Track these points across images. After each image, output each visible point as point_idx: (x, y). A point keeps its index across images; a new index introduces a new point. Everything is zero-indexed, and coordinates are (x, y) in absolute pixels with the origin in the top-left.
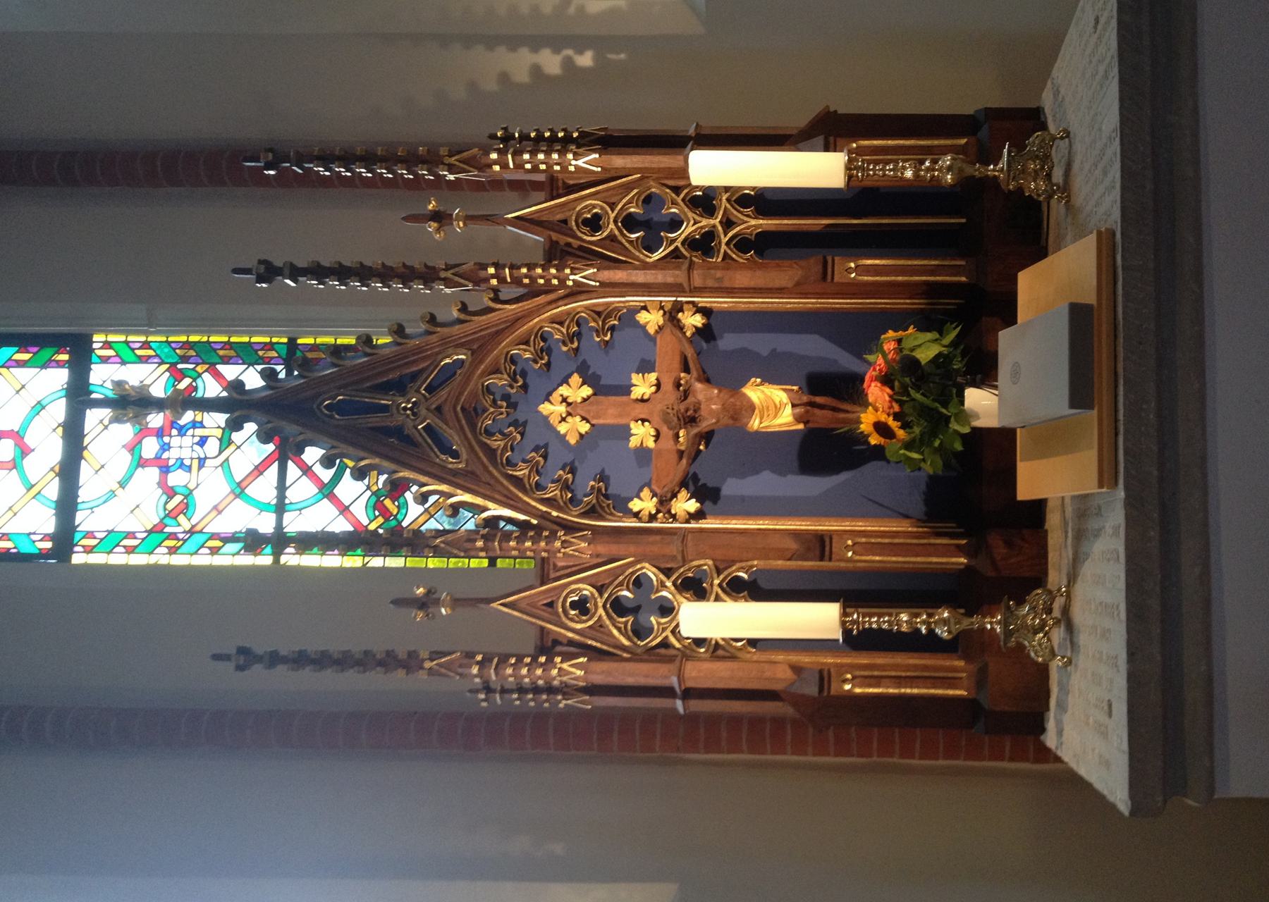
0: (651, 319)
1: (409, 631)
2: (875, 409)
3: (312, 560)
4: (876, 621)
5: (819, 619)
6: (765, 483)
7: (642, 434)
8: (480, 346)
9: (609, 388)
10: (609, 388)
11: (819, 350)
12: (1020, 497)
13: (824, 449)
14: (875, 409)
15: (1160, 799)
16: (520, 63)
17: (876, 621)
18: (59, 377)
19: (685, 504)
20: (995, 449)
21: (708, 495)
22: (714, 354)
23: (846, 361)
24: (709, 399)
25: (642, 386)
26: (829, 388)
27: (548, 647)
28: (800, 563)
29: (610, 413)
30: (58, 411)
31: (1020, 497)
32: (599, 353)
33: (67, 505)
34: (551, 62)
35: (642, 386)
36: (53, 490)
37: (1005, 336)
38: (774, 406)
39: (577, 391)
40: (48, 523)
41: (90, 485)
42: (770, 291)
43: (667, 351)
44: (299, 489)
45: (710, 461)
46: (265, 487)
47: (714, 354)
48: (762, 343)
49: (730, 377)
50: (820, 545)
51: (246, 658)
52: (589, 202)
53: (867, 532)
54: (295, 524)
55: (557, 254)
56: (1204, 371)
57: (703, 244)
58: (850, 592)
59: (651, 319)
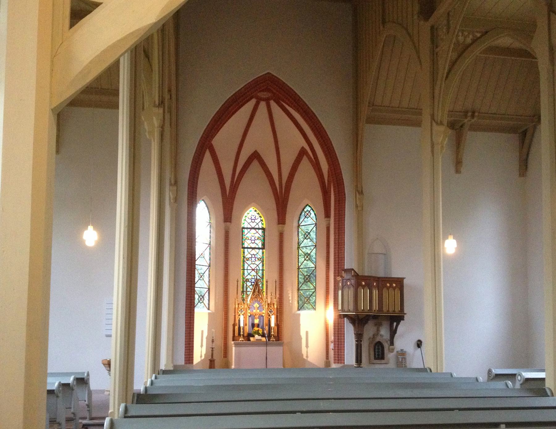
0: (263, 311)
2: (256, 329)
6: (251, 320)
7: (254, 311)
8: (261, 298)
12: (90, 228)
13: (253, 325)
14: (256, 329)
15: (441, 138)
16: (290, 295)
18: (260, 246)
19: (249, 315)
20: (253, 336)
22: (261, 316)
23: (260, 326)
24: (257, 316)
25: (258, 311)
26: (258, 326)
27: (238, 304)
29: (256, 308)
30: (257, 247)
31: (90, 228)
33: (247, 248)
34: (290, 298)
35: (258, 311)
36: (249, 246)
37: (455, 375)
38: (256, 321)
39: (258, 306)
40: (246, 246)
41: (250, 250)
42: (266, 321)
43: (261, 313)
45: (252, 316)
48: (262, 320)
49: (259, 318)
50: (246, 325)
52: (272, 306)
53: (247, 329)
54: (246, 271)
55: (268, 304)
57: (269, 316)
59: (263, 311)
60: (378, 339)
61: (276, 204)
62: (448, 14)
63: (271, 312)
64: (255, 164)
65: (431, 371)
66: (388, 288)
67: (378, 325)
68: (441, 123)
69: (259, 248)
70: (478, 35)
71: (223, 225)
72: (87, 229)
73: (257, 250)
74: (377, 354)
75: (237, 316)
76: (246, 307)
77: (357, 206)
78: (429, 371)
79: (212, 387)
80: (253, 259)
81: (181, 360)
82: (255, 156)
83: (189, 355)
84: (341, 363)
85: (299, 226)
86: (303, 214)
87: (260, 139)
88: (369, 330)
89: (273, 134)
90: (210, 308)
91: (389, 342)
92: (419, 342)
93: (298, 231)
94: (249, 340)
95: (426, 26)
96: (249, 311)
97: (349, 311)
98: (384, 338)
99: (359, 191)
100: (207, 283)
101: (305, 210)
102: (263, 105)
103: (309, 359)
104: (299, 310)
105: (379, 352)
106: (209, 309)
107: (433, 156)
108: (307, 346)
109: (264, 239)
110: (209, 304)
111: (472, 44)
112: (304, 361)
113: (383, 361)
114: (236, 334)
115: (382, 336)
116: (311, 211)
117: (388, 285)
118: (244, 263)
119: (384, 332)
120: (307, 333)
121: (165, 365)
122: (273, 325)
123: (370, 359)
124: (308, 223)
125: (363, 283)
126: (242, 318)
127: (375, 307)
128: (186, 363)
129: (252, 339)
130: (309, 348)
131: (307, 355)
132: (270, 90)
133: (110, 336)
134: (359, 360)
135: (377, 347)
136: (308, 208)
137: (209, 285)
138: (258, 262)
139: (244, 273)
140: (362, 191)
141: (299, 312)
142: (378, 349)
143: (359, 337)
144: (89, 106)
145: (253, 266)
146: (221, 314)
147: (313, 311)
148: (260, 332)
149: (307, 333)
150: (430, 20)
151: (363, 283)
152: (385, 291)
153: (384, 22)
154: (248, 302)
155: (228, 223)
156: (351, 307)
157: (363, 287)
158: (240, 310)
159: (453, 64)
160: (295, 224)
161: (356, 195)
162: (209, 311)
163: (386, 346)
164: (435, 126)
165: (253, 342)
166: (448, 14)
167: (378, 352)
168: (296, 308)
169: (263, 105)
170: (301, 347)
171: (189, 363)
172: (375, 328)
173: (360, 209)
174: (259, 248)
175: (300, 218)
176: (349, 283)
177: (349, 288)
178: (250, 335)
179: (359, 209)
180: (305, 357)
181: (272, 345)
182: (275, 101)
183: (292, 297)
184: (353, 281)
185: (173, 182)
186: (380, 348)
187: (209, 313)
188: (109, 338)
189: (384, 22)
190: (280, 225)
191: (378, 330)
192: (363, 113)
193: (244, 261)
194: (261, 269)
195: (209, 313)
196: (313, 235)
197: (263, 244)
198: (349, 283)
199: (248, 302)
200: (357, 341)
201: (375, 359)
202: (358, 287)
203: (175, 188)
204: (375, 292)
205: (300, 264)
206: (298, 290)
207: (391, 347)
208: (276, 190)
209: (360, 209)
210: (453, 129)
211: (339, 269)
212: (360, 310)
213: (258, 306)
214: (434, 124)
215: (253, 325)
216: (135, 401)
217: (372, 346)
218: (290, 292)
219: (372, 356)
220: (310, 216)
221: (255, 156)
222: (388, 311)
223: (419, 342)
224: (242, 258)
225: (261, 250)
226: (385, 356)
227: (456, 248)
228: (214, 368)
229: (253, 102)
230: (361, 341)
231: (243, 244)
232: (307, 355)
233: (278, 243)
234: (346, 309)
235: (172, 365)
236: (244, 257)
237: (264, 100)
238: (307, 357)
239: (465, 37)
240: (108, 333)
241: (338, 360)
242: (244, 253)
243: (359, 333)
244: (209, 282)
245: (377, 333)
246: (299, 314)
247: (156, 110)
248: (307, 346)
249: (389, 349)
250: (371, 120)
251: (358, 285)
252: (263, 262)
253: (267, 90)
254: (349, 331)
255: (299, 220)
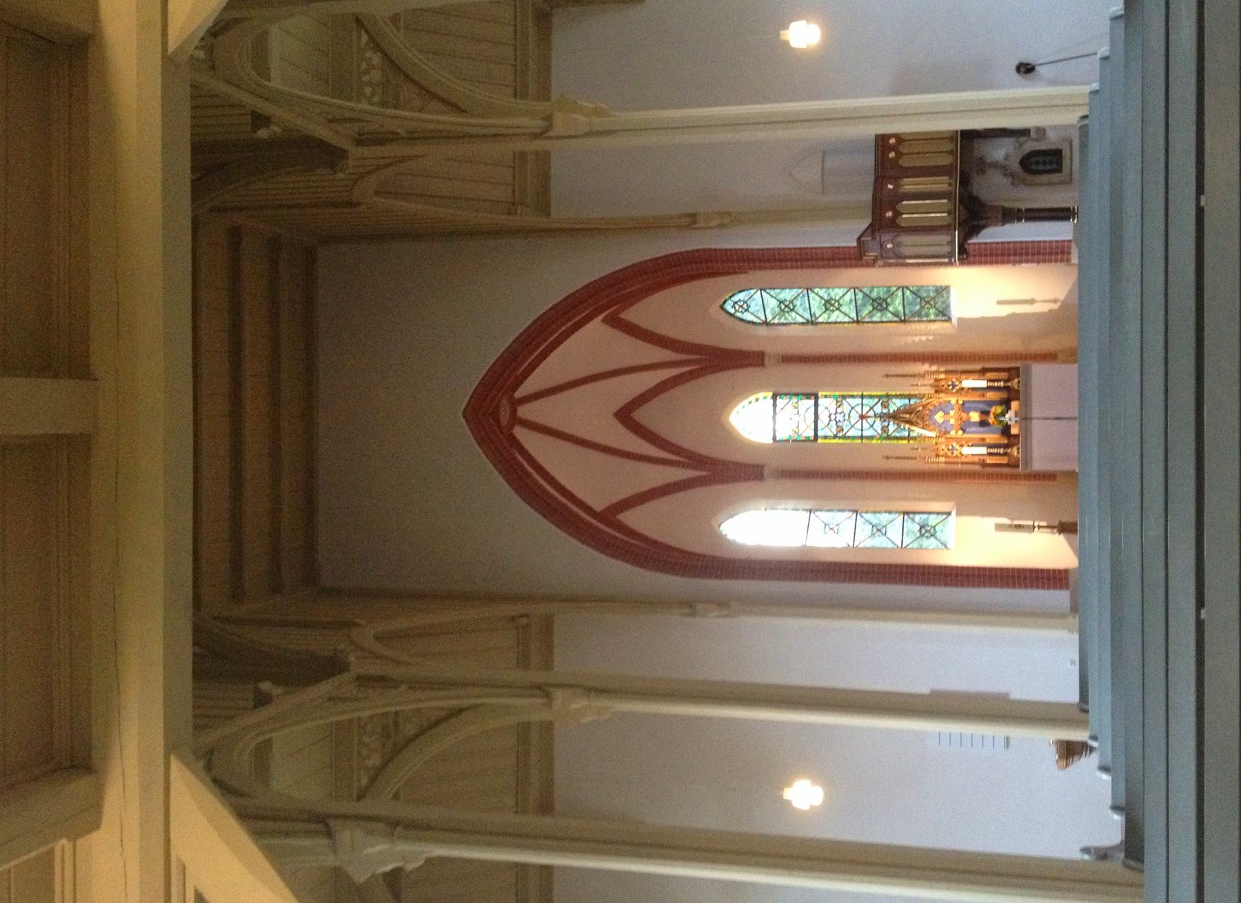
1: (913, 454)
3: (827, 441)
4: (992, 451)
5: (983, 450)
6: (974, 429)
7: (952, 421)
8: (924, 407)
9: (946, 413)
10: (946, 413)
11: (982, 406)
13: (983, 423)
15: (578, 116)
16: (917, 339)
17: (992, 451)
18: (812, 402)
19: (960, 432)
21: (964, 431)
22: (964, 408)
23: (987, 408)
24: (964, 415)
25: (952, 413)
26: (985, 413)
27: (937, 456)
28: (890, 98)
32: (945, 408)
34: (924, 338)
35: (952, 413)
36: (813, 426)
38: (975, 417)
41: (820, 425)
43: (956, 407)
44: (866, 426)
45: (964, 426)
46: (858, 426)
47: (964, 408)
50: (983, 439)
51: (888, 458)
52: (943, 383)
53: (993, 437)
54: (865, 434)
56: (551, 654)
58: (989, 446)
60: (1015, 165)
61: (721, 370)
62: (330, 121)
63: (954, 386)
64: (642, 415)
65: (1085, 117)
66: (900, 155)
67: (982, 166)
68: (549, 118)
69: (816, 405)
70: (365, 38)
71: (770, 483)
72: (789, 802)
73: (820, 409)
74: (1048, 167)
75: (963, 459)
76: (942, 440)
77: (722, 226)
78: (1086, 122)
79: (1115, 674)
80: (840, 417)
81: (1059, 598)
82: (625, 415)
83: (1049, 579)
84: (1069, 247)
85: (766, 323)
86: (738, 314)
87: (589, 412)
88: (994, 189)
89: (578, 401)
90: (947, 510)
91: (1022, 139)
92: (1022, 69)
93: (779, 324)
94: (1017, 436)
95: (355, 151)
96: (953, 433)
97: (952, 243)
98: (1011, 151)
99: (691, 221)
100: (894, 516)
101: (732, 311)
102: (524, 412)
103: (1061, 295)
104: (949, 320)
105: (1044, 161)
106: (949, 514)
107: (616, 131)
108: (1032, 302)
109: (797, 395)
110: (938, 513)
111: (382, 51)
112: (1065, 306)
113: (1066, 153)
114: (1005, 460)
115: (1007, 157)
116: (735, 298)
117: (892, 155)
118: (849, 438)
119: (999, 151)
120: (999, 303)
121: (1071, 631)
122: (983, 384)
123: (1061, 183)
124: (757, 305)
125: (889, 214)
126: (967, 451)
127: (941, 184)
128: (1067, 587)
129: (1014, 431)
130: (1037, 297)
131: (1050, 301)
132: (494, 413)
133: (1007, 739)
134: (1062, 214)
135: (1033, 167)
136: (728, 306)
137: (896, 512)
138: (846, 408)
139: (871, 438)
140: (690, 215)
141: (954, 320)
142: (1037, 163)
143: (1010, 215)
144: (550, 770)
145: (855, 417)
146: (961, 487)
147: (953, 291)
148: (999, 409)
149: (999, 303)
150: (344, 147)
151: (889, 214)
152: (905, 162)
153: (351, 204)
154: (933, 434)
155: (766, 472)
156: (944, 238)
157: (897, 214)
158: (949, 453)
159: (427, 92)
160: (763, 331)
161: (699, 228)
162: (954, 513)
163: (1030, 146)
164: (558, 130)
165: (1020, 429)
166: (330, 121)
167: (1044, 163)
168: (946, 325)
169: (524, 412)
170: (1034, 314)
171: (1067, 579)
172: (990, 172)
173: (729, 219)
174: (816, 405)
175: (749, 322)
176: (890, 246)
177: (899, 245)
178: (1006, 430)
179: (727, 221)
180: (1056, 306)
181: (1027, 385)
182: (515, 389)
183: (923, 334)
184: (885, 237)
185: (686, 610)
186: (1033, 160)
187: (959, 514)
188: (1012, 742)
189: (351, 204)
190: (767, 361)
191: (996, 165)
192: (529, 213)
193: (845, 437)
194: (859, 400)
195: (959, 514)
196: (787, 294)
197: (808, 396)
198: (890, 246)
199: (933, 434)
200: (1019, 220)
201: (1059, 170)
202: (898, 226)
203: (700, 607)
204: (909, 185)
205: (847, 319)
206: (904, 321)
207: (1033, 134)
208: (691, 372)
209: (729, 219)
210: (550, 15)
211: (854, 257)
212: (950, 220)
213: (941, 414)
214: (551, 134)
215: (983, 423)
216: (1138, 865)
217: (1029, 177)
218: (910, 339)
219: (1054, 177)
220: (745, 302)
221: (625, 415)
222: (950, 152)
223: (1022, 69)
224: (837, 441)
225: (821, 401)
226: (1053, 147)
227: (808, 21)
228: (1075, 524)
229: (520, 433)
230: (1019, 210)
231: (807, 440)
232: (1050, 301)
233: (804, 365)
234: (947, 249)
235: (1070, 619)
236: (835, 437)
237: (514, 412)
238: (1055, 301)
239: (374, 67)
240: (1000, 742)
241: (1063, 253)
242: (826, 437)
243: (1000, 216)
244: (890, 512)
245: (1003, 169)
246: (960, 320)
247: (558, 702)
248: (1032, 302)
249: (1036, 140)
250: (544, 207)
251: (893, 226)
252: (844, 397)
253: (495, 415)
254: (994, 234)
255: (754, 323)
